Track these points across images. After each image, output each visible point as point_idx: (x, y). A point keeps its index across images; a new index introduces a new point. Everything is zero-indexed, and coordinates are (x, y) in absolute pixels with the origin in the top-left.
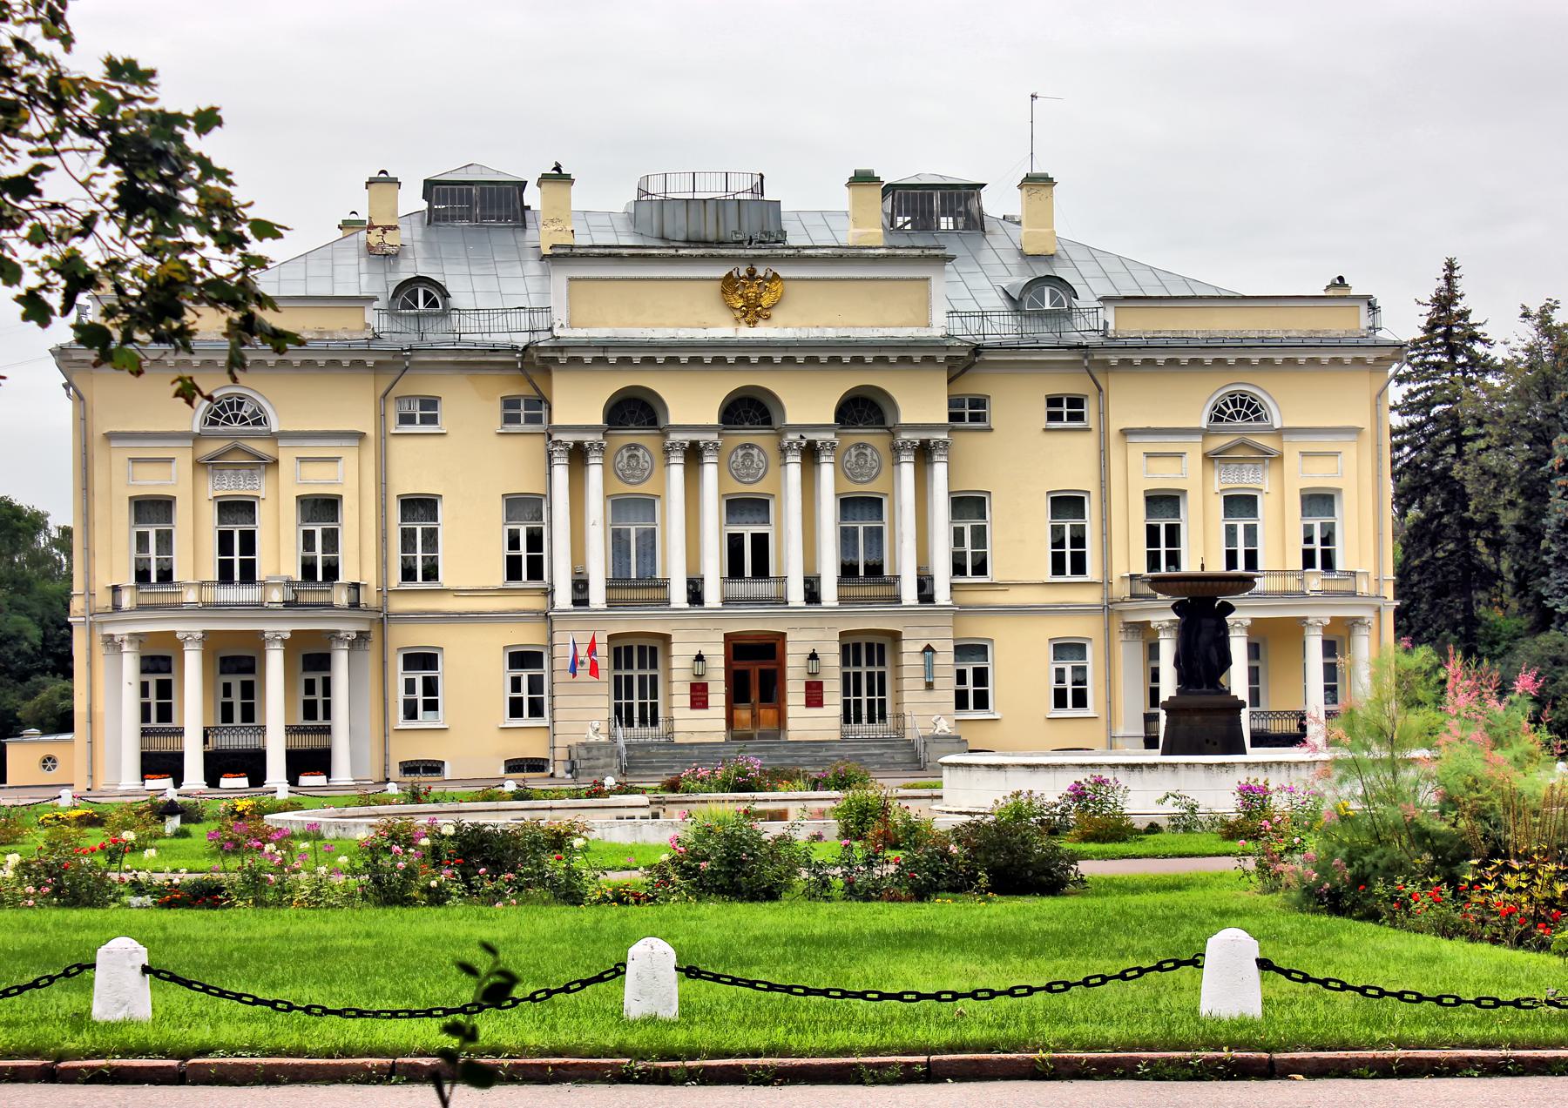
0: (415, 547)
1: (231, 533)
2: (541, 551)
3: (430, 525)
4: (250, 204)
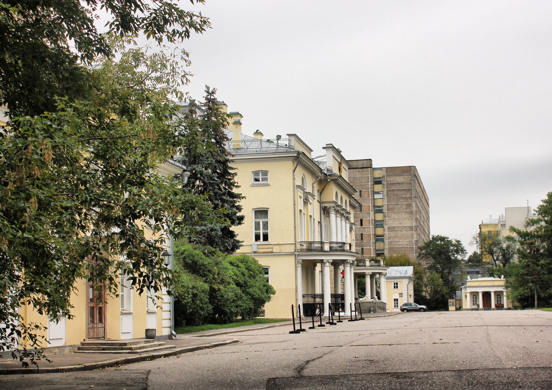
2: (260, 230)
3: (265, 220)
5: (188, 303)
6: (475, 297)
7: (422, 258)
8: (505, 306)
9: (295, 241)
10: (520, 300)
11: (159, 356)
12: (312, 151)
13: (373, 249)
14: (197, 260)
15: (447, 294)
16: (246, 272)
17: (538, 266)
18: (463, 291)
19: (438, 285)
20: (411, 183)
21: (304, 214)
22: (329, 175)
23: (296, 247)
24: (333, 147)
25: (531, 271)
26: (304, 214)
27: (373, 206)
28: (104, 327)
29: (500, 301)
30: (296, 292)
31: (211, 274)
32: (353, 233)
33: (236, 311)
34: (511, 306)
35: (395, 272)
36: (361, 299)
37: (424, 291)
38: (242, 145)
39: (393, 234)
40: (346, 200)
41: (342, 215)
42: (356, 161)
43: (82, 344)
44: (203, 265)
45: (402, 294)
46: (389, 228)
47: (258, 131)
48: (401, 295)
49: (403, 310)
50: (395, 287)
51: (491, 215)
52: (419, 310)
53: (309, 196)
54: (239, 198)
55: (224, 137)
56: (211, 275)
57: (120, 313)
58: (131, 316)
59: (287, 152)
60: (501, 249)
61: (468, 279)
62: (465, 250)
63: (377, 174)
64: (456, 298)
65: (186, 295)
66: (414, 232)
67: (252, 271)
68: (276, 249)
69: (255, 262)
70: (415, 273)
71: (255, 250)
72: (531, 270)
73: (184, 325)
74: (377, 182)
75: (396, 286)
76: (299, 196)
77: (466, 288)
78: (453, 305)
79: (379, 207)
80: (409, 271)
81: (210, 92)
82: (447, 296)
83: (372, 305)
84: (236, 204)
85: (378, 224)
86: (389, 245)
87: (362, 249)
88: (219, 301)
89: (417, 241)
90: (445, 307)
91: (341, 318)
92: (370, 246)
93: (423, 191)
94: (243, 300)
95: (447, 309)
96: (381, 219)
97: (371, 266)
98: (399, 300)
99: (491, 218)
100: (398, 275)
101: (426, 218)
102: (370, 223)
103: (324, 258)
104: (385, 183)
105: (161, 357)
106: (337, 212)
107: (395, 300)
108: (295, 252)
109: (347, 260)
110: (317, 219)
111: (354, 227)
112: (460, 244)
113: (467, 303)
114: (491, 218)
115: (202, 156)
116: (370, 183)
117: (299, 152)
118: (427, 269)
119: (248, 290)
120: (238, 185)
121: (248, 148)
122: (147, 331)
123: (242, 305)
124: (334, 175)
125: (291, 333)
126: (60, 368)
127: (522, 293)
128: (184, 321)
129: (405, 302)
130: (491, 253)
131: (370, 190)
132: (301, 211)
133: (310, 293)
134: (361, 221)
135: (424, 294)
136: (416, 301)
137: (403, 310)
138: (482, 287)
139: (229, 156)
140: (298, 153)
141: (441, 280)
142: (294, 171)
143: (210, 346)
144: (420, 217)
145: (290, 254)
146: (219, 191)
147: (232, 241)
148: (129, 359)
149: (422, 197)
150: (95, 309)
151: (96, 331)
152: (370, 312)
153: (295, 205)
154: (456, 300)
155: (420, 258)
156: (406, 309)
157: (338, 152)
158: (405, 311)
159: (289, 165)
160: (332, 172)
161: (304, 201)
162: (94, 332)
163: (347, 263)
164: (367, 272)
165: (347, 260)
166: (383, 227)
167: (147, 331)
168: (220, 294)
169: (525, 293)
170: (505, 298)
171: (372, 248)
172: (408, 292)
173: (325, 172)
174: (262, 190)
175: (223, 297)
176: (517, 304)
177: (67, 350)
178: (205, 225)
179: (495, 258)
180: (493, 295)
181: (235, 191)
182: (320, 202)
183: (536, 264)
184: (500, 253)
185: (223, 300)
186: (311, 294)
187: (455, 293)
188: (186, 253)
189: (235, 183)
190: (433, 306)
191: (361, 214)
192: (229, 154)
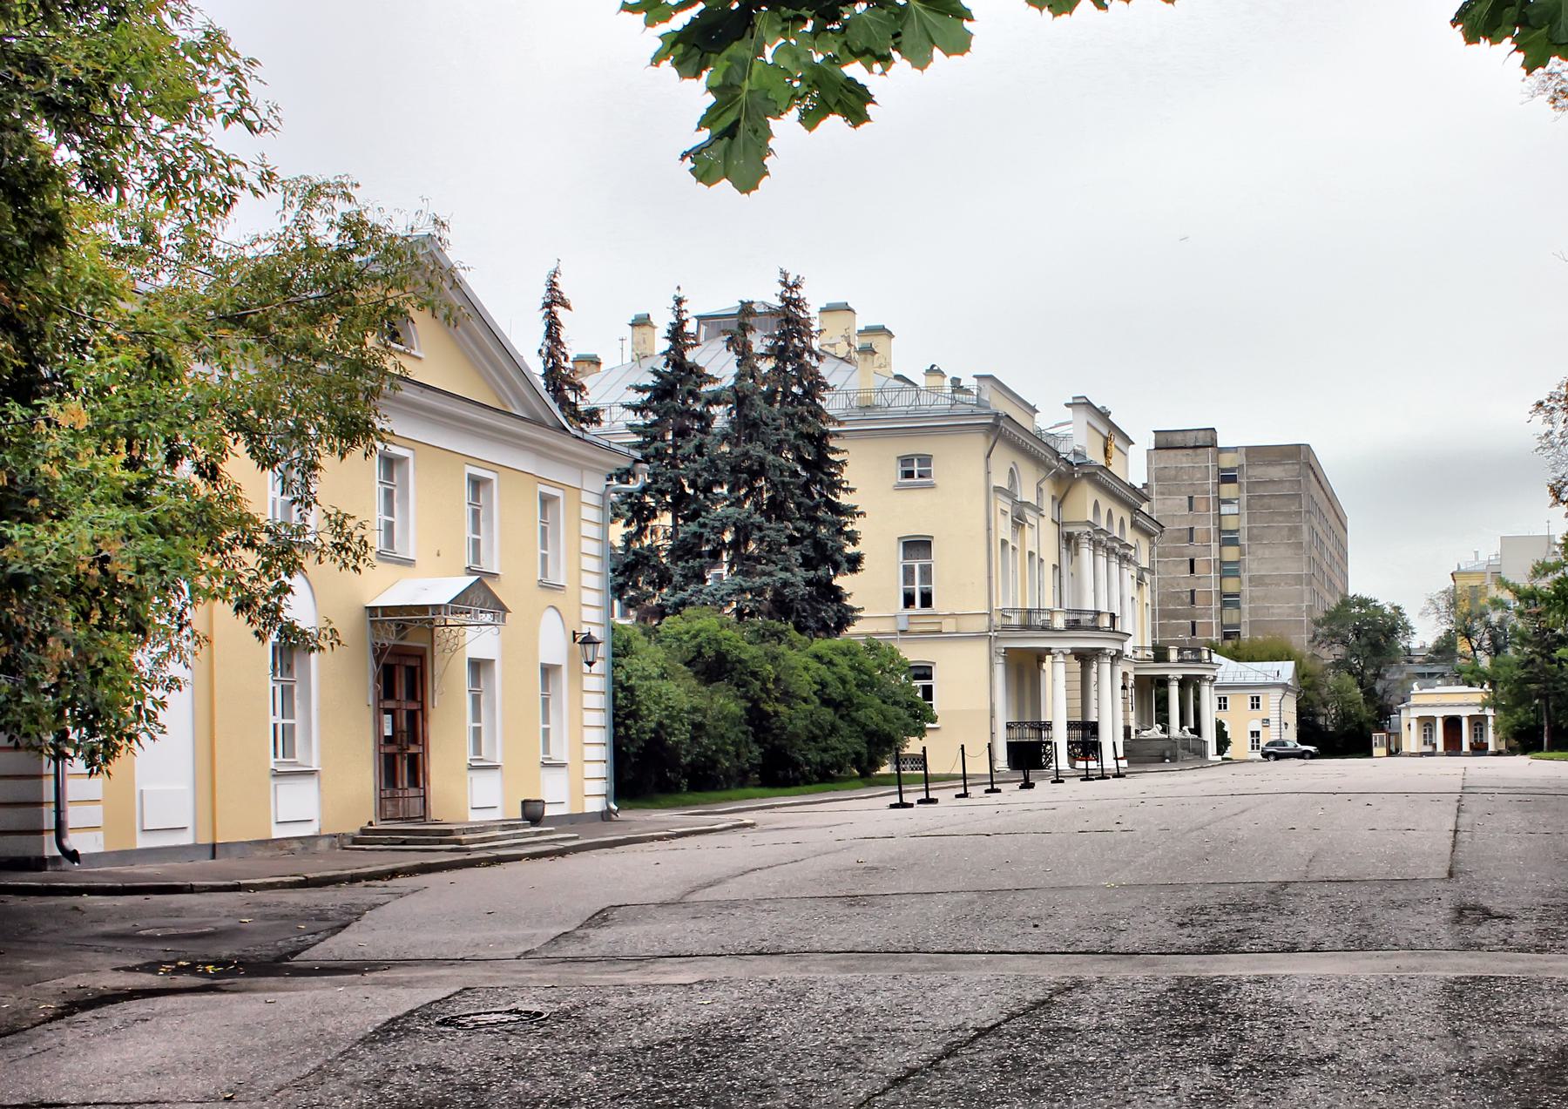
0: (913, 580)
1: (912, 568)
2: (914, 584)
3: (925, 562)
4: (236, 456)
5: (683, 743)
6: (1427, 728)
7: (1320, 643)
8: (1491, 748)
9: (990, 608)
10: (1518, 735)
11: (518, 858)
12: (1037, 411)
14: (728, 651)
15: (1369, 720)
16: (850, 675)
17: (1552, 662)
20: (1300, 481)
21: (1014, 548)
23: (991, 620)
24: (1089, 404)
25: (1536, 674)
26: (1014, 548)
27: (1217, 531)
28: (424, 796)
29: (1481, 736)
31: (757, 680)
32: (1146, 589)
33: (819, 760)
34: (1503, 748)
35: (1254, 674)
36: (1145, 733)
37: (1322, 714)
38: (877, 399)
39: (1259, 591)
40: (1122, 520)
41: (1110, 551)
42: (1181, 434)
43: (364, 831)
44: (740, 661)
45: (1268, 720)
47: (935, 368)
48: (1266, 722)
49: (1266, 755)
50: (1253, 707)
51: (1476, 552)
52: (1302, 755)
53: (1027, 511)
54: (852, 515)
55: (818, 382)
56: (758, 683)
57: (465, 767)
58: (497, 773)
59: (973, 415)
60: (1488, 625)
61: (1413, 689)
62: (1411, 628)
63: (1227, 461)
64: (1390, 731)
65: (676, 726)
66: (1305, 587)
67: (866, 674)
68: (948, 626)
69: (894, 652)
70: (1301, 674)
72: (1536, 670)
73: (685, 790)
74: (1227, 478)
77: (1408, 707)
78: (1381, 745)
79: (1231, 532)
80: (1286, 670)
81: (791, 284)
82: (1368, 726)
83: (1169, 744)
84: (846, 529)
85: (1227, 570)
86: (1250, 614)
87: (1193, 624)
88: (776, 736)
89: (1310, 608)
90: (1365, 751)
91: (1090, 772)
93: (1331, 499)
94: (842, 736)
95: (1369, 754)
96: (1235, 559)
97: (1179, 661)
98: (1261, 734)
99: (1477, 558)
100: (1261, 680)
101: (1337, 557)
104: (1244, 481)
105: (520, 860)
106: (1096, 544)
107: (1252, 733)
110: (1050, 558)
111: (1147, 577)
112: (1401, 614)
113: (1411, 740)
114: (1477, 558)
115: (766, 425)
116: (1211, 481)
119: (854, 714)
120: (850, 486)
121: (889, 406)
122: (525, 803)
123: (838, 746)
124: (1089, 464)
125: (893, 806)
126: (242, 882)
127: (1522, 719)
128: (685, 782)
130: (1468, 635)
131: (1211, 495)
132: (1004, 543)
134: (1192, 562)
135: (1321, 721)
136: (1302, 739)
137: (1266, 755)
138: (1443, 705)
139: (831, 424)
141: (1359, 690)
142: (989, 456)
143: (667, 836)
144: (1321, 554)
145: (978, 636)
146: (808, 501)
147: (835, 608)
148: (430, 864)
149: (1328, 511)
150: (399, 758)
151: (400, 803)
153: (989, 529)
155: (1316, 643)
156: (1276, 753)
157: (1103, 415)
158: (1272, 758)
159: (978, 444)
162: (396, 806)
164: (1171, 673)
165: (1104, 649)
167: (525, 803)
168: (778, 724)
169: (1529, 719)
170: (1490, 730)
173: (1071, 458)
174: (919, 498)
175: (785, 728)
176: (1514, 743)
177: (323, 845)
178: (770, 574)
179: (1475, 644)
180: (1465, 723)
181: (844, 499)
182: (1058, 524)
183: (1548, 658)
184: (1486, 635)
185: (785, 737)
186: (1032, 723)
187: (1390, 719)
188: (703, 635)
189: (843, 482)
192: (831, 419)
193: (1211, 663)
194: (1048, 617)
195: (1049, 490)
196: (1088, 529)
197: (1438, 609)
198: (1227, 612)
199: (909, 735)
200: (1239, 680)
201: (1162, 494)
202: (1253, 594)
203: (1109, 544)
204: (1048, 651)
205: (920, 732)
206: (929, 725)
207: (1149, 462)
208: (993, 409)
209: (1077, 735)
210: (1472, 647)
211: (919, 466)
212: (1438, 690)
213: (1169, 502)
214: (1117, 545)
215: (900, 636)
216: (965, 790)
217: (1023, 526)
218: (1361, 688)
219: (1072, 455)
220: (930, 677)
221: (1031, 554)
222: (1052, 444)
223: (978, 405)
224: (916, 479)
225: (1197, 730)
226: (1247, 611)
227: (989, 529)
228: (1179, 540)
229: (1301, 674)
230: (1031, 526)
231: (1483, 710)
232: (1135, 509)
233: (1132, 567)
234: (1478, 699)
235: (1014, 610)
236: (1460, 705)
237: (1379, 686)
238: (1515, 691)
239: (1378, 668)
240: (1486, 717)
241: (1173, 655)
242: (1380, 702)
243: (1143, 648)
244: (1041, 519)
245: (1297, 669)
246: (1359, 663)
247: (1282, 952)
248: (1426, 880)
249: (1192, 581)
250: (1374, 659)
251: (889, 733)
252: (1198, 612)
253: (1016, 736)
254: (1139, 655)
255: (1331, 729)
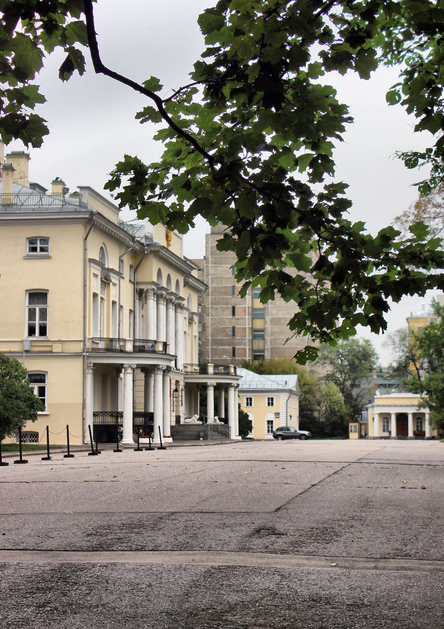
0: (35, 318)
1: (35, 310)
2: (35, 320)
8: (427, 435)
13: (249, 349)
15: (348, 414)
18: (370, 410)
19: (335, 402)
21: (102, 299)
22: (147, 245)
23: (85, 345)
26: (102, 299)
29: (421, 426)
30: (84, 407)
34: (435, 433)
35: (270, 383)
37: (317, 410)
38: (14, 200)
40: (177, 282)
45: (279, 413)
46: (272, 320)
47: (59, 180)
48: (277, 415)
52: (300, 437)
53: (111, 274)
61: (375, 394)
64: (361, 422)
68: (57, 348)
70: (301, 383)
71: (27, 348)
75: (271, 402)
76: (92, 275)
77: (373, 407)
83: (203, 428)
86: (271, 343)
87: (234, 349)
92: (245, 345)
95: (347, 437)
97: (215, 374)
100: (275, 387)
102: (245, 311)
103: (125, 362)
106: (159, 297)
108: (84, 352)
109: (158, 365)
112: (369, 345)
117: (92, 212)
118: (323, 380)
124: (155, 245)
129: (283, 425)
132: (95, 295)
133: (109, 409)
134: (234, 309)
135: (316, 414)
137: (276, 437)
138: (395, 406)
140: (92, 213)
141: (341, 395)
142: (86, 239)
145: (76, 355)
152: (198, 439)
153: (85, 286)
154: (361, 424)
160: (152, 240)
161: (101, 280)
163: (159, 369)
166: (264, 318)
170: (427, 423)
171: (247, 348)
172: (287, 412)
173: (143, 241)
180: (410, 419)
182: (134, 283)
187: (361, 414)
190: (327, 431)
191: (234, 299)
193: (236, 375)
194: (122, 344)
195: (127, 261)
196: (153, 287)
197: (394, 342)
198: (256, 342)
199: (26, 419)
200: (260, 387)
201: (215, 263)
202: (273, 330)
203: (168, 297)
204: (122, 365)
205: (34, 417)
206: (39, 413)
207: (207, 242)
208: (89, 208)
209: (140, 421)
210: (417, 368)
211: (41, 244)
212: (392, 395)
213: (219, 269)
214: (173, 298)
215: (24, 354)
216: (48, 455)
217: (109, 284)
218: (343, 393)
219: (144, 239)
220: (44, 381)
221: (114, 303)
222: (131, 232)
223: (80, 206)
224: (39, 253)
225: (226, 420)
226: (269, 341)
227: (85, 286)
228: (226, 293)
229: (302, 382)
230: (115, 284)
231: (419, 409)
232: (187, 274)
233: (184, 311)
234: (416, 402)
235: (101, 339)
236: (407, 406)
237: (355, 392)
238: (440, 397)
239: (354, 379)
240: (424, 414)
241: (211, 370)
242: (355, 403)
243: (192, 365)
244: (122, 280)
245: (299, 380)
246: (341, 377)
247: (134, 550)
248: (258, 513)
249: (233, 321)
250: (351, 374)
251: (8, 417)
252: (237, 341)
253: (100, 420)
254: (189, 369)
255: (322, 420)
